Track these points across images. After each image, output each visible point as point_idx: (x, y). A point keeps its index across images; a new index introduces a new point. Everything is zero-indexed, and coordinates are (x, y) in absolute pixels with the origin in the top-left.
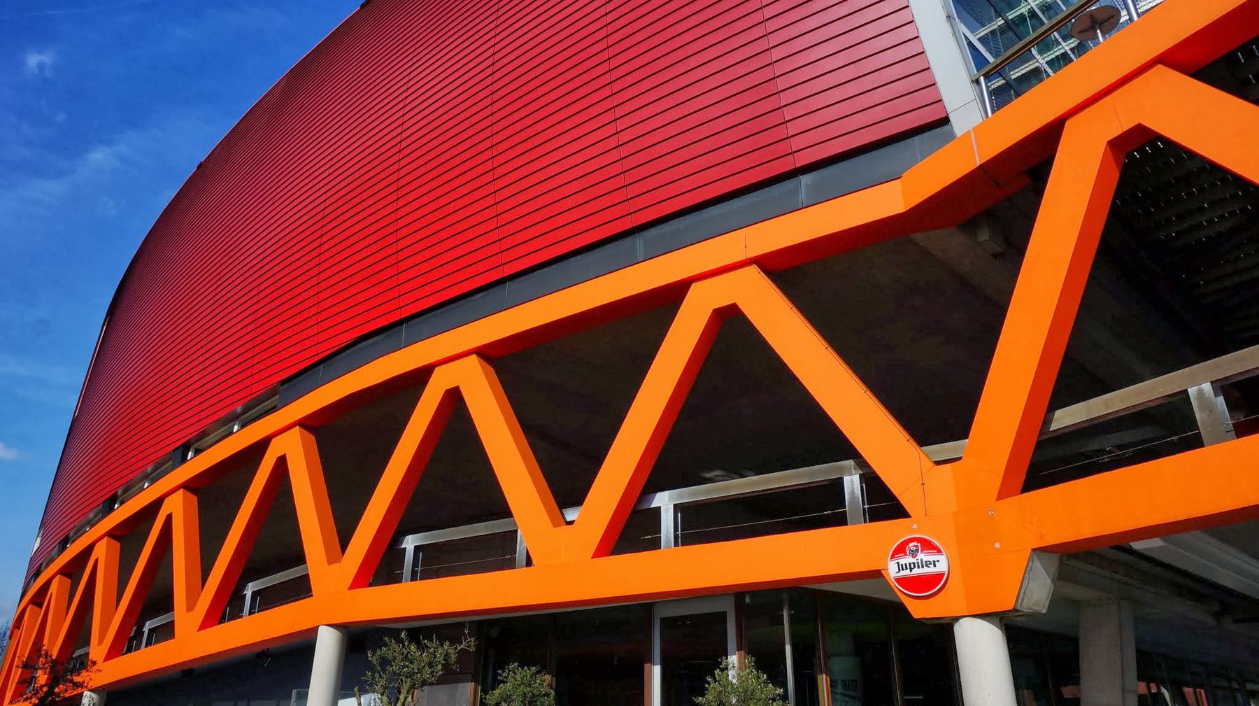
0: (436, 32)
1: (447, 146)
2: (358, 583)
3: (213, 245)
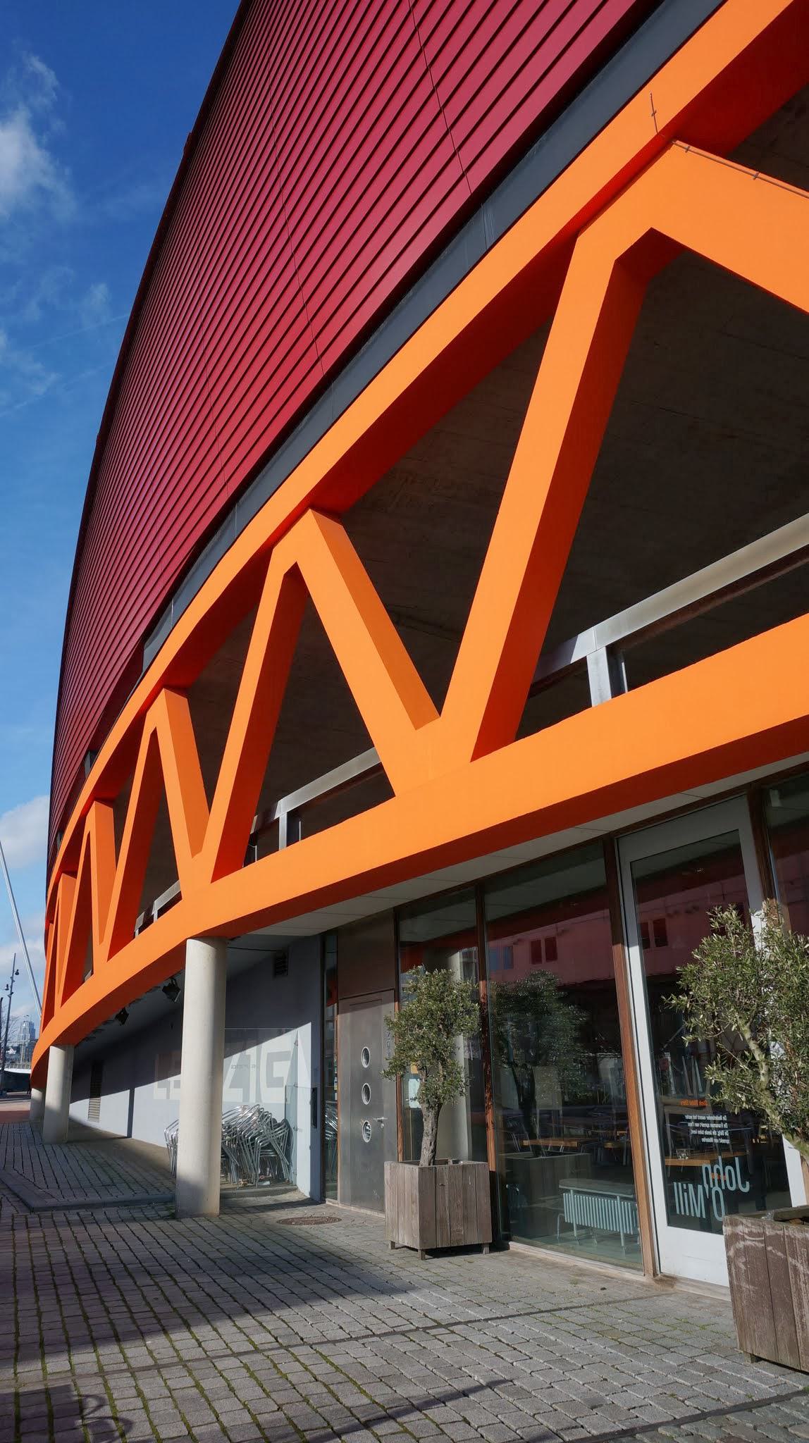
0: (236, 155)
1: (92, 714)
2: (489, 742)
3: (188, 248)
